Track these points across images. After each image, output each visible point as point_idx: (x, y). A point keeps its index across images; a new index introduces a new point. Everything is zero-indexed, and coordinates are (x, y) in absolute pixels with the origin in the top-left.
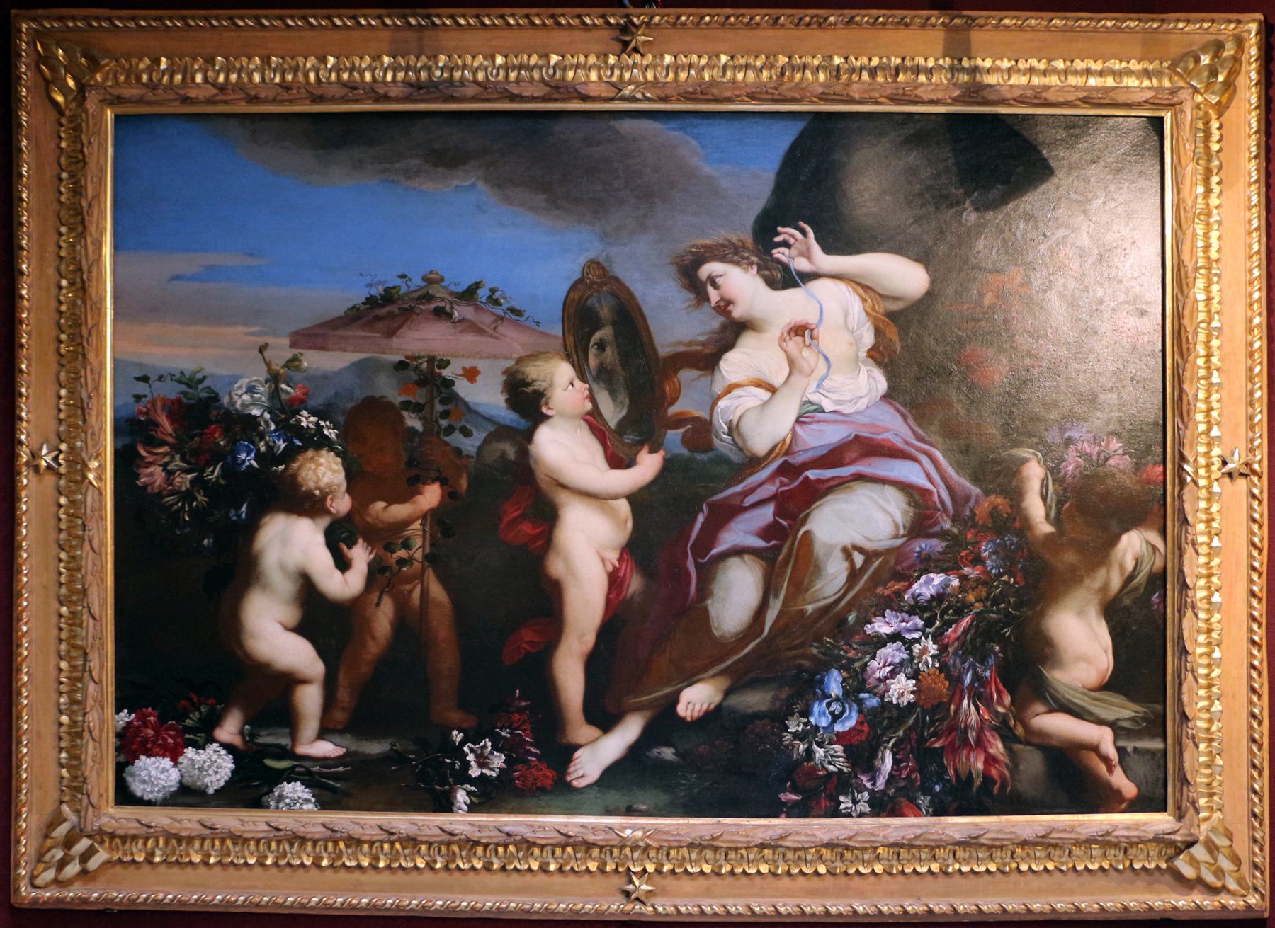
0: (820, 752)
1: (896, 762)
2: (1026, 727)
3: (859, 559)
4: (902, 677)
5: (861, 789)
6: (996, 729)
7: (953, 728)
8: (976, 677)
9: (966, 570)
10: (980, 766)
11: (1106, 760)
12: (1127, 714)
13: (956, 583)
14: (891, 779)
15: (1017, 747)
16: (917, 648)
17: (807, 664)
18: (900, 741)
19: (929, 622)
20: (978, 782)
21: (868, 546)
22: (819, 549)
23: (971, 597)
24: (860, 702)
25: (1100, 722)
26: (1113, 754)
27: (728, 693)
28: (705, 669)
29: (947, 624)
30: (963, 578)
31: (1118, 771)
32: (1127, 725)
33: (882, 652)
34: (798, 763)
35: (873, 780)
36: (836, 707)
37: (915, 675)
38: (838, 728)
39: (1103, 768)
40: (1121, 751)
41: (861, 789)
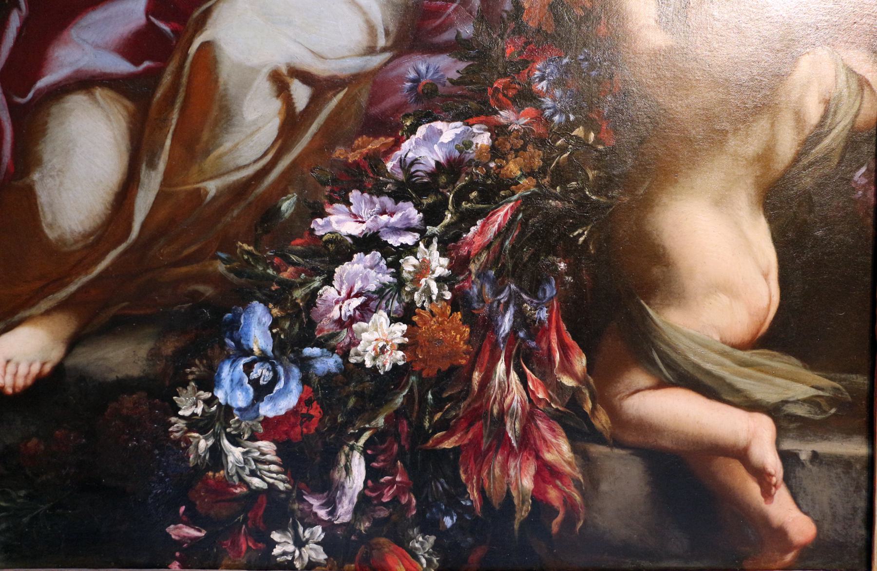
0: (234, 454)
1: (372, 474)
2: (614, 413)
3: (301, 94)
4: (381, 318)
5: (312, 520)
6: (557, 417)
7: (477, 414)
8: (522, 320)
9: (505, 116)
10: (528, 483)
11: (760, 474)
12: (802, 391)
13: (484, 139)
14: (363, 503)
15: (597, 450)
16: (409, 264)
17: (208, 290)
18: (379, 436)
19: (432, 215)
20: (523, 512)
21: (320, 68)
22: (226, 73)
23: (513, 168)
24: (305, 364)
25: (752, 406)
26: (773, 463)
27: (73, 344)
28: (30, 301)
29: (467, 219)
30: (498, 131)
31: (782, 495)
32: (801, 411)
33: (344, 270)
34: (198, 471)
35: (331, 505)
36: (261, 372)
37: (407, 314)
38: (266, 410)
39: (754, 489)
40: (787, 458)
41: (312, 520)
